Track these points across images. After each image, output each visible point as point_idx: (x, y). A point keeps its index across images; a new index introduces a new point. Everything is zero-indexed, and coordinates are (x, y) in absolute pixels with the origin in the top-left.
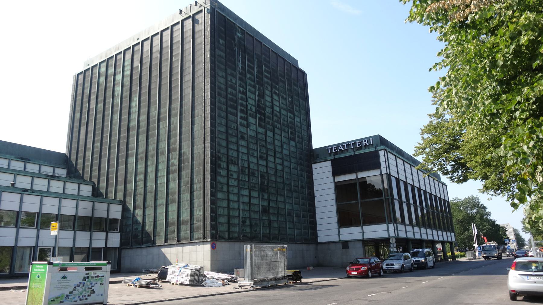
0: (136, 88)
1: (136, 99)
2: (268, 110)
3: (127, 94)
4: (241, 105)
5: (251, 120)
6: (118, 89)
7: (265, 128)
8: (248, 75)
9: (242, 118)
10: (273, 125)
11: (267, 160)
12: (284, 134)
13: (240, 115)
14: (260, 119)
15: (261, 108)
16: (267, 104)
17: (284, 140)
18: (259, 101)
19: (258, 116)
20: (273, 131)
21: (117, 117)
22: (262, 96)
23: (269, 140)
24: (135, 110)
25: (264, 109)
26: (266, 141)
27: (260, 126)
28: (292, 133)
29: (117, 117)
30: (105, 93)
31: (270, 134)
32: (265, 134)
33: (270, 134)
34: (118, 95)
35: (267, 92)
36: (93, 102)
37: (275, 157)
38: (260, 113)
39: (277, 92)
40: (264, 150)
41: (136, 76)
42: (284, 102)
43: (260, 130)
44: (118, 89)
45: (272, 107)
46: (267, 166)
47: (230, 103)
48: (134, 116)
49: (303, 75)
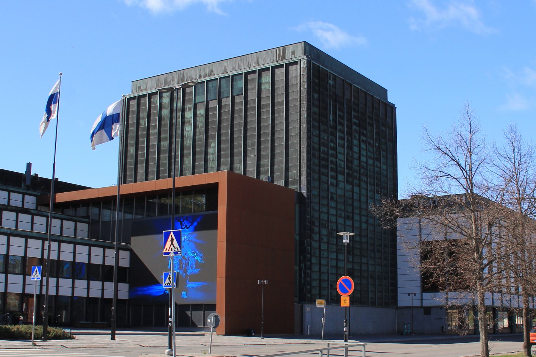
0: (213, 132)
2: (356, 162)
4: (332, 162)
6: (189, 129)
7: (352, 184)
8: (339, 127)
9: (332, 177)
10: (360, 179)
11: (353, 219)
12: (369, 187)
14: (348, 174)
15: (349, 161)
16: (356, 156)
17: (370, 194)
18: (348, 154)
19: (346, 171)
20: (359, 186)
22: (350, 148)
23: (356, 197)
25: (352, 162)
26: (352, 198)
27: (348, 182)
31: (356, 189)
33: (356, 189)
35: (355, 142)
37: (360, 214)
38: (348, 168)
39: (365, 139)
41: (214, 119)
43: (349, 187)
44: (189, 129)
45: (359, 159)
47: (323, 163)
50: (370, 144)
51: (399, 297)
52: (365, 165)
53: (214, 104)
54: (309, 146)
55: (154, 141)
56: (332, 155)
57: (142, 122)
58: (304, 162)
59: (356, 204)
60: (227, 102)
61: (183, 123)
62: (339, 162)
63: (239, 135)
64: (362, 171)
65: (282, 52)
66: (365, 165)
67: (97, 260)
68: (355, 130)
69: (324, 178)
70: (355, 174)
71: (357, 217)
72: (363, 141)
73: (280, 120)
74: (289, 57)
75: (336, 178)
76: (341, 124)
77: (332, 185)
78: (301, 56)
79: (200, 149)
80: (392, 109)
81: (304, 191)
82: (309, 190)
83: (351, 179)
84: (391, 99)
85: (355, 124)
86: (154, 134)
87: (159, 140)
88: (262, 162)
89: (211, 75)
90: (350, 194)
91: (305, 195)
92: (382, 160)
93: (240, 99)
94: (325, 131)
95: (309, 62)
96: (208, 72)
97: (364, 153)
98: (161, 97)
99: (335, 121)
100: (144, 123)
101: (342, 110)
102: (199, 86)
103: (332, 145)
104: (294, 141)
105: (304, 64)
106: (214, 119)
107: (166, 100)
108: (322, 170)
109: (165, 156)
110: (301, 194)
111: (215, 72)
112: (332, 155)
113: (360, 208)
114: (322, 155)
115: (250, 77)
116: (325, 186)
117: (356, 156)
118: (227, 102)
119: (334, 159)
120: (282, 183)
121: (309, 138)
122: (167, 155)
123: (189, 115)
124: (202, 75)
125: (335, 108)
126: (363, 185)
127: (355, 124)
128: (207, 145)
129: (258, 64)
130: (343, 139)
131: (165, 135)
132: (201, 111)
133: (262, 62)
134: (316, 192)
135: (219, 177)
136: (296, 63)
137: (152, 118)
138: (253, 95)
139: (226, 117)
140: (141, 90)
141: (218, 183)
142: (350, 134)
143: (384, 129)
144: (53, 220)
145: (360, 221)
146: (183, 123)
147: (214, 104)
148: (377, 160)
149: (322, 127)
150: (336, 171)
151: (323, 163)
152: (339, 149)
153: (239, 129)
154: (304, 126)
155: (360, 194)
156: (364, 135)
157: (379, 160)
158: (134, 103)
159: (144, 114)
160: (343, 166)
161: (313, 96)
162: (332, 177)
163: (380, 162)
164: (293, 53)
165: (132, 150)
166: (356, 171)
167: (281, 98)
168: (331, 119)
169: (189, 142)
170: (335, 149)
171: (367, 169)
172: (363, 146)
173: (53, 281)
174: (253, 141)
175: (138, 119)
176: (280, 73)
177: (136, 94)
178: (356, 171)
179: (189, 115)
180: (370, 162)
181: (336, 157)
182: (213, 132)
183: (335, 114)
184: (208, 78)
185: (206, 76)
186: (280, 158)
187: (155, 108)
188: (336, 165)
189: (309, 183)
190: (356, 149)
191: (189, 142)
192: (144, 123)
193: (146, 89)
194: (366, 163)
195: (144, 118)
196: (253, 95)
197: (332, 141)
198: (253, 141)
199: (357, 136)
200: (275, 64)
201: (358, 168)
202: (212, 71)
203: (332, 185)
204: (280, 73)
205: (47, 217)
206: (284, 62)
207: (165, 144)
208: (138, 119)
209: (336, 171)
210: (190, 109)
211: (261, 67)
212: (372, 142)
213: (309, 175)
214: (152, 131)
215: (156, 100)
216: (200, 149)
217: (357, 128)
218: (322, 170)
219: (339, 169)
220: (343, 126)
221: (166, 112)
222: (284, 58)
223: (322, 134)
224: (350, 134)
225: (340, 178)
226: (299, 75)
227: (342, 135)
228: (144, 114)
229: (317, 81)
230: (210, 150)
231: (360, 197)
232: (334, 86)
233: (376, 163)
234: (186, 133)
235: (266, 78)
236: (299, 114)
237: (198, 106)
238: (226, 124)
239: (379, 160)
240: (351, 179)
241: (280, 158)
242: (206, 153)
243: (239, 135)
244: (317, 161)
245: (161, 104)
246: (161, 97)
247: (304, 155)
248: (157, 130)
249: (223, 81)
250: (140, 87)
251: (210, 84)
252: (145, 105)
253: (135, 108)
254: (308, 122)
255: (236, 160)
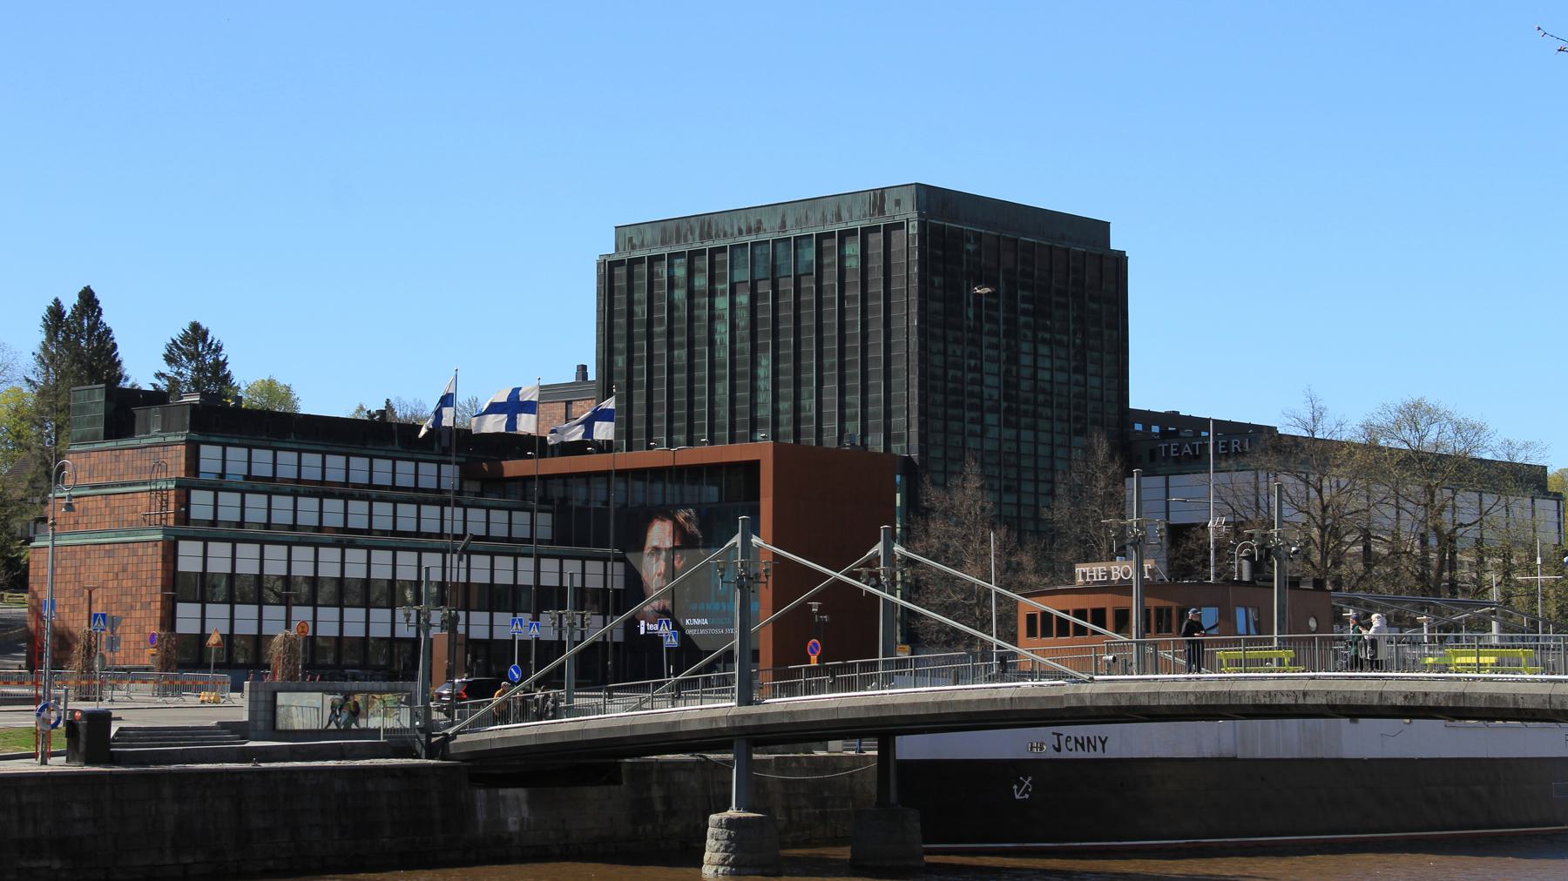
0: (766, 340)
1: (765, 363)
2: (1025, 385)
3: (744, 346)
4: (971, 394)
5: (990, 419)
6: (723, 329)
7: (1017, 426)
8: (987, 327)
9: (972, 421)
10: (1036, 415)
11: (1018, 491)
12: (1058, 426)
13: (968, 415)
14: (1008, 410)
15: (1010, 385)
16: (1025, 372)
17: (1058, 439)
18: (1007, 372)
19: (1004, 405)
20: (1034, 428)
21: (723, 389)
22: (1014, 359)
23: (1025, 449)
24: (765, 384)
25: (1017, 387)
26: (1018, 453)
27: (1008, 424)
28: (1077, 419)
29: (723, 389)
30: (690, 329)
31: (1027, 435)
32: (1018, 440)
33: (1027, 435)
34: (1244, 869)
35: (1025, 347)
36: (660, 342)
37: (1036, 481)
38: (1007, 398)
39: (1047, 336)
40: (1013, 473)
41: (765, 315)
42: (1063, 353)
43: (1009, 433)
44: (723, 329)
45: (1034, 377)
46: (1019, 505)
47: (952, 398)
48: (765, 397)
49: (1119, 262)
52: (1048, 386)
53: (765, 288)
55: (661, 350)
56: (973, 382)
57: (637, 309)
58: (915, 403)
59: (1027, 462)
60: (787, 285)
61: (712, 318)
62: (986, 392)
65: (878, 198)
66: (1048, 386)
68: (1026, 325)
71: (1028, 487)
72: (1043, 341)
73: (877, 328)
74: (893, 214)
75: (981, 421)
76: (990, 319)
77: (972, 434)
78: (909, 214)
81: (915, 455)
83: (1013, 419)
84: (1115, 244)
85: (1025, 312)
86: (660, 335)
87: (671, 347)
88: (848, 398)
89: (758, 230)
90: (1013, 445)
91: (916, 460)
92: (1091, 368)
93: (809, 283)
94: (957, 341)
95: (922, 225)
96: (753, 224)
98: (671, 266)
99: (978, 317)
100: (641, 311)
102: (738, 252)
103: (973, 362)
104: (898, 366)
105: (913, 231)
106: (765, 315)
107: (680, 272)
108: (950, 411)
111: (765, 225)
112: (973, 382)
113: (1036, 468)
115: (826, 243)
116: (959, 439)
117: (1025, 372)
118: (787, 285)
119: (977, 388)
123: (722, 303)
124: (744, 228)
127: (1025, 312)
128: (754, 363)
129: (839, 218)
130: (996, 347)
131: (681, 338)
132: (743, 299)
133: (845, 215)
134: (937, 453)
135: (761, 449)
136: (900, 226)
138: (830, 279)
140: (633, 247)
143: (1095, 306)
144: (540, 515)
145: (1036, 493)
146: (712, 318)
147: (765, 288)
148: (1076, 370)
149: (951, 335)
151: (952, 398)
152: (987, 367)
154: (914, 339)
155: (1036, 442)
157: (1081, 370)
158: (621, 272)
159: (641, 295)
160: (996, 397)
162: (972, 421)
163: (1085, 374)
164: (898, 203)
165: (620, 361)
166: (1027, 402)
167: (877, 288)
168: (971, 315)
169: (723, 355)
175: (631, 303)
176: (876, 240)
177: (625, 256)
178: (1027, 402)
179: (722, 303)
180: (1060, 377)
181: (981, 383)
182: (766, 340)
185: (749, 231)
187: (661, 285)
188: (981, 398)
189: (923, 438)
190: (1026, 360)
191: (723, 355)
193: (642, 245)
194: (1051, 382)
195: (661, 419)
196: (830, 279)
197: (971, 356)
199: (1029, 334)
200: (866, 223)
202: (760, 222)
203: (972, 434)
204: (876, 240)
205: (532, 512)
207: (681, 354)
208: (631, 303)
209: (980, 408)
210: (723, 293)
211: (843, 227)
212: (1065, 338)
215: (662, 270)
217: (1031, 320)
219: (987, 404)
220: (997, 322)
221: (680, 294)
222: (882, 212)
223: (951, 348)
225: (990, 419)
226: (906, 244)
227: (995, 340)
228: (641, 295)
229: (940, 253)
230: (761, 372)
231: (1036, 449)
234: (718, 337)
235: (853, 248)
237: (738, 287)
238: (787, 326)
239: (1081, 370)
240: (1013, 419)
242: (754, 378)
245: (671, 278)
246: (671, 266)
247: (915, 391)
248: (664, 328)
249: (780, 246)
250: (631, 239)
252: (641, 278)
253: (624, 283)
254: (922, 332)
255: (804, 391)
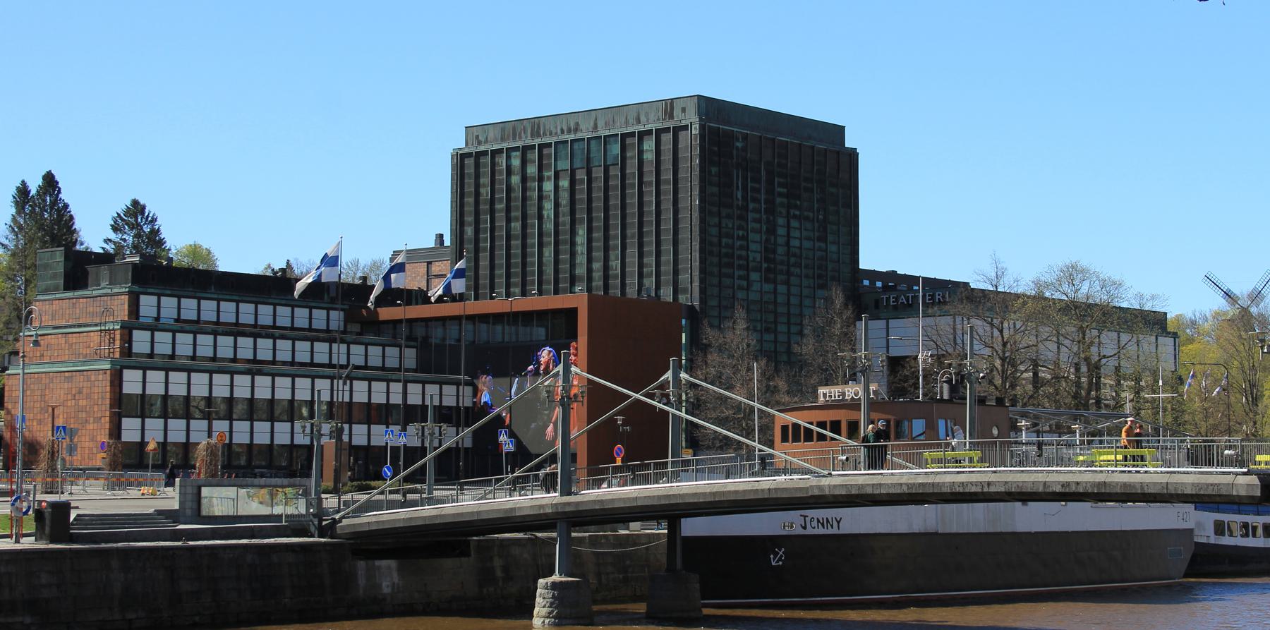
0: (582, 215)
2: (780, 250)
4: (740, 257)
6: (549, 207)
7: (775, 282)
8: (751, 206)
9: (740, 278)
10: (788, 273)
11: (775, 332)
15: (769, 250)
16: (781, 241)
19: (765, 265)
20: (787, 283)
22: (772, 231)
23: (780, 299)
25: (774, 252)
26: (775, 302)
27: (767, 280)
31: (782, 289)
33: (782, 289)
35: (781, 221)
37: (789, 324)
38: (767, 260)
41: (582, 196)
43: (768, 287)
44: (549, 207)
45: (788, 244)
47: (725, 260)
50: (807, 218)
51: (141, 308)
53: (581, 175)
54: (703, 241)
56: (741, 248)
57: (482, 190)
58: (697, 264)
60: (598, 173)
61: (541, 198)
62: (751, 255)
63: (616, 222)
64: (793, 260)
65: (669, 106)
67: (379, 398)
69: (727, 281)
70: (779, 267)
72: (795, 217)
74: (680, 118)
75: (747, 278)
77: (740, 288)
79: (565, 237)
80: (853, 155)
81: (696, 304)
82: (703, 301)
85: (780, 195)
87: (509, 220)
88: (645, 260)
89: (576, 130)
90: (772, 296)
92: (830, 238)
94: (728, 216)
95: (702, 127)
96: (572, 125)
97: (796, 234)
98: (508, 157)
99: (745, 198)
100: (485, 192)
101: (756, 180)
104: (684, 235)
105: (696, 131)
106: (582, 196)
107: (516, 162)
109: (516, 243)
110: (692, 307)
111: (582, 126)
112: (741, 248)
114: (724, 250)
117: (781, 241)
119: (744, 253)
120: (667, 294)
121: (703, 231)
122: (519, 242)
123: (548, 186)
124: (565, 129)
125: (745, 179)
126: (794, 280)
128: (573, 233)
129: (638, 121)
131: (516, 214)
132: (564, 183)
133: (643, 119)
135: (578, 299)
136: (685, 128)
137: (497, 186)
138: (632, 168)
139: (598, 194)
140: (479, 143)
141: (576, 309)
142: (771, 211)
143: (833, 190)
146: (541, 198)
147: (581, 175)
148: (819, 239)
149: (724, 212)
150: (747, 268)
151: (725, 260)
152: (752, 236)
153: (616, 213)
154: (696, 215)
155: (789, 294)
156: (796, 207)
157: (823, 239)
158: (470, 162)
159: (485, 180)
161: (710, 172)
162: (740, 278)
164: (684, 110)
165: (469, 231)
167: (667, 175)
168: (739, 196)
169: (549, 226)
170: (745, 238)
171: (801, 257)
172: (794, 224)
173: (301, 439)
174: (633, 231)
175: (477, 186)
176: (667, 138)
177: (472, 150)
179: (548, 186)
180: (807, 244)
182: (582, 215)
183: (745, 188)
184: (572, 136)
185: (569, 131)
186: (668, 257)
187: (501, 172)
189: (703, 291)
190: (781, 231)
191: (549, 226)
192: (485, 192)
193: (486, 141)
196: (632, 168)
198: (633, 231)
200: (659, 126)
201: (785, 258)
202: (577, 124)
203: (740, 288)
204: (667, 138)
206: (671, 124)
207: (516, 226)
208: (477, 186)
209: (747, 268)
210: (549, 178)
211: (641, 128)
212: (811, 215)
213: (702, 281)
214: (498, 206)
215: (502, 161)
216: (565, 237)
217: (785, 200)
218: (724, 270)
219: (751, 264)
221: (516, 179)
222: (671, 117)
223: (724, 221)
224: (771, 211)
225: (754, 276)
226: (690, 142)
227: (757, 216)
228: (485, 180)
232: (744, 149)
233: (817, 244)
234: (545, 213)
235: (649, 145)
236: (691, 199)
237: (561, 174)
238: (598, 204)
239: (823, 239)
241: (668, 257)
242: (573, 244)
243: (616, 222)
244: (715, 260)
246: (508, 157)
247: (697, 255)
249: (593, 143)
250: (477, 137)
251: (576, 146)
255: (612, 254)
